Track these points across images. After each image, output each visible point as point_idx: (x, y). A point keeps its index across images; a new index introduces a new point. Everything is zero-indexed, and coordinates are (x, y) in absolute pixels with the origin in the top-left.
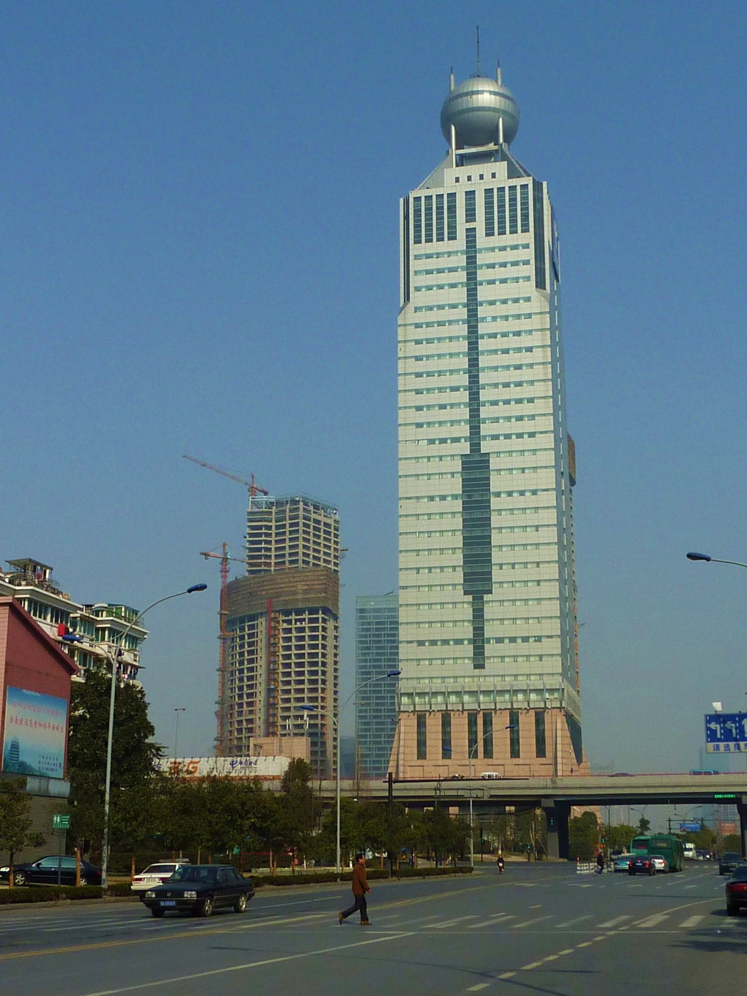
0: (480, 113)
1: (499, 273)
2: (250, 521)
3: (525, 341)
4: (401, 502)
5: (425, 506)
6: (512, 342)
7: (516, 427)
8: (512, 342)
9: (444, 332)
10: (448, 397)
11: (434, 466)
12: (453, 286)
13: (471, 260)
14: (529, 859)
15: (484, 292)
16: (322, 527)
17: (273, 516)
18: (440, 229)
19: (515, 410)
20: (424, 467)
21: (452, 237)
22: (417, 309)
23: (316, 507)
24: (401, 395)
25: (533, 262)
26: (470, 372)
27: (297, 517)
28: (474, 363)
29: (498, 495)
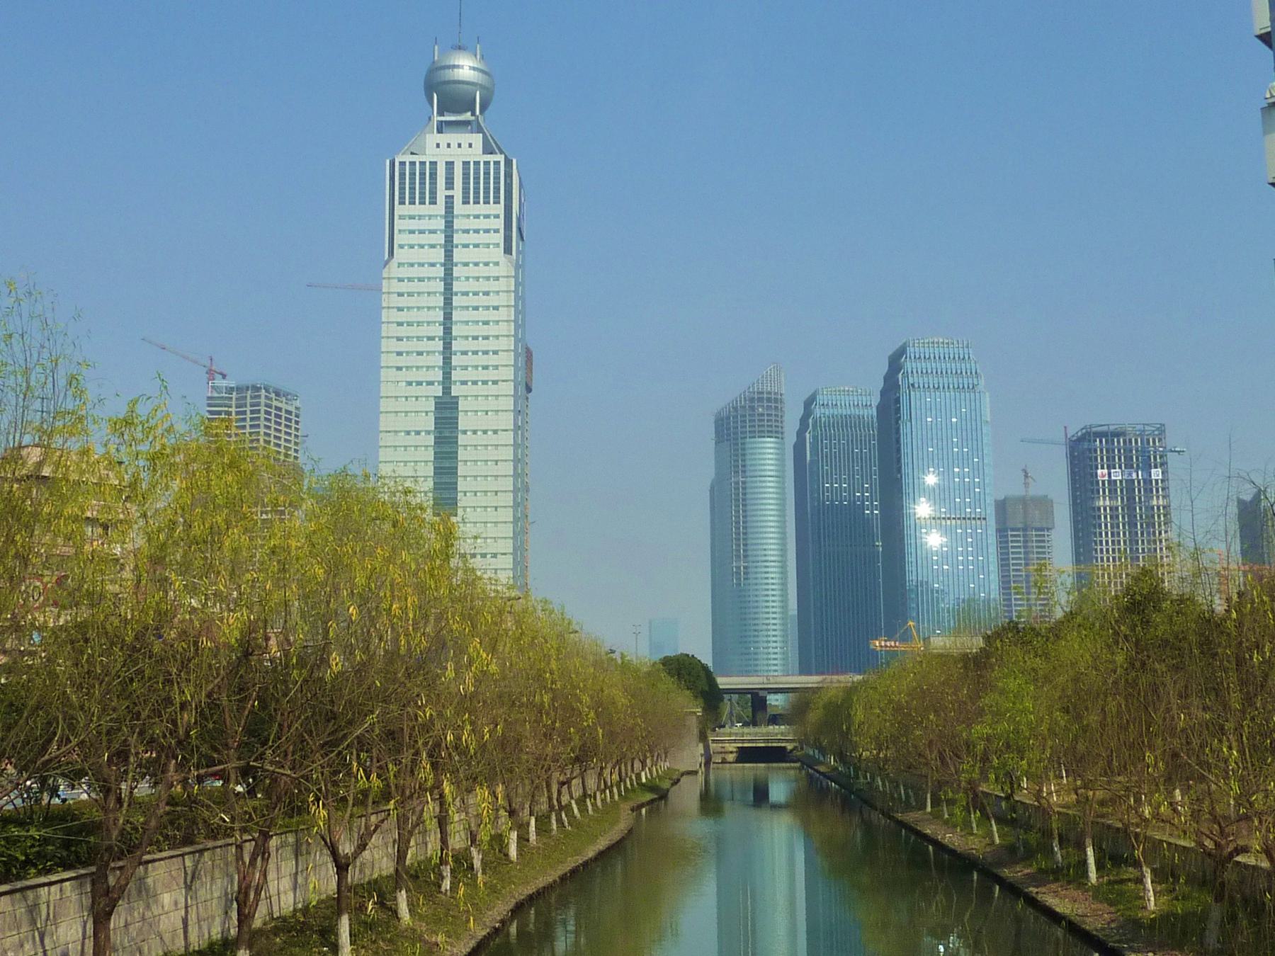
0: (460, 86)
1: (472, 238)
2: (209, 405)
3: (493, 300)
4: (382, 435)
5: (402, 439)
6: (482, 300)
7: (481, 375)
8: (482, 300)
9: (423, 287)
10: (424, 346)
11: (411, 405)
12: (433, 246)
13: (449, 224)
14: (106, 798)
15: (458, 255)
16: (283, 414)
17: (234, 403)
18: (422, 194)
19: (481, 360)
20: (402, 405)
21: (433, 201)
22: (400, 265)
23: (277, 394)
24: (384, 341)
25: (502, 231)
26: (444, 339)
27: (258, 404)
28: (448, 317)
29: (465, 432)
